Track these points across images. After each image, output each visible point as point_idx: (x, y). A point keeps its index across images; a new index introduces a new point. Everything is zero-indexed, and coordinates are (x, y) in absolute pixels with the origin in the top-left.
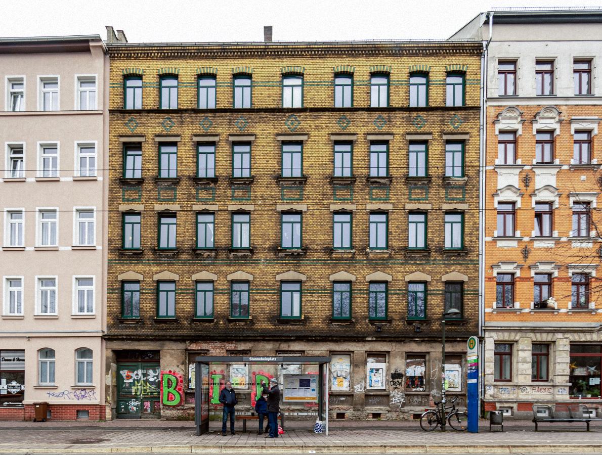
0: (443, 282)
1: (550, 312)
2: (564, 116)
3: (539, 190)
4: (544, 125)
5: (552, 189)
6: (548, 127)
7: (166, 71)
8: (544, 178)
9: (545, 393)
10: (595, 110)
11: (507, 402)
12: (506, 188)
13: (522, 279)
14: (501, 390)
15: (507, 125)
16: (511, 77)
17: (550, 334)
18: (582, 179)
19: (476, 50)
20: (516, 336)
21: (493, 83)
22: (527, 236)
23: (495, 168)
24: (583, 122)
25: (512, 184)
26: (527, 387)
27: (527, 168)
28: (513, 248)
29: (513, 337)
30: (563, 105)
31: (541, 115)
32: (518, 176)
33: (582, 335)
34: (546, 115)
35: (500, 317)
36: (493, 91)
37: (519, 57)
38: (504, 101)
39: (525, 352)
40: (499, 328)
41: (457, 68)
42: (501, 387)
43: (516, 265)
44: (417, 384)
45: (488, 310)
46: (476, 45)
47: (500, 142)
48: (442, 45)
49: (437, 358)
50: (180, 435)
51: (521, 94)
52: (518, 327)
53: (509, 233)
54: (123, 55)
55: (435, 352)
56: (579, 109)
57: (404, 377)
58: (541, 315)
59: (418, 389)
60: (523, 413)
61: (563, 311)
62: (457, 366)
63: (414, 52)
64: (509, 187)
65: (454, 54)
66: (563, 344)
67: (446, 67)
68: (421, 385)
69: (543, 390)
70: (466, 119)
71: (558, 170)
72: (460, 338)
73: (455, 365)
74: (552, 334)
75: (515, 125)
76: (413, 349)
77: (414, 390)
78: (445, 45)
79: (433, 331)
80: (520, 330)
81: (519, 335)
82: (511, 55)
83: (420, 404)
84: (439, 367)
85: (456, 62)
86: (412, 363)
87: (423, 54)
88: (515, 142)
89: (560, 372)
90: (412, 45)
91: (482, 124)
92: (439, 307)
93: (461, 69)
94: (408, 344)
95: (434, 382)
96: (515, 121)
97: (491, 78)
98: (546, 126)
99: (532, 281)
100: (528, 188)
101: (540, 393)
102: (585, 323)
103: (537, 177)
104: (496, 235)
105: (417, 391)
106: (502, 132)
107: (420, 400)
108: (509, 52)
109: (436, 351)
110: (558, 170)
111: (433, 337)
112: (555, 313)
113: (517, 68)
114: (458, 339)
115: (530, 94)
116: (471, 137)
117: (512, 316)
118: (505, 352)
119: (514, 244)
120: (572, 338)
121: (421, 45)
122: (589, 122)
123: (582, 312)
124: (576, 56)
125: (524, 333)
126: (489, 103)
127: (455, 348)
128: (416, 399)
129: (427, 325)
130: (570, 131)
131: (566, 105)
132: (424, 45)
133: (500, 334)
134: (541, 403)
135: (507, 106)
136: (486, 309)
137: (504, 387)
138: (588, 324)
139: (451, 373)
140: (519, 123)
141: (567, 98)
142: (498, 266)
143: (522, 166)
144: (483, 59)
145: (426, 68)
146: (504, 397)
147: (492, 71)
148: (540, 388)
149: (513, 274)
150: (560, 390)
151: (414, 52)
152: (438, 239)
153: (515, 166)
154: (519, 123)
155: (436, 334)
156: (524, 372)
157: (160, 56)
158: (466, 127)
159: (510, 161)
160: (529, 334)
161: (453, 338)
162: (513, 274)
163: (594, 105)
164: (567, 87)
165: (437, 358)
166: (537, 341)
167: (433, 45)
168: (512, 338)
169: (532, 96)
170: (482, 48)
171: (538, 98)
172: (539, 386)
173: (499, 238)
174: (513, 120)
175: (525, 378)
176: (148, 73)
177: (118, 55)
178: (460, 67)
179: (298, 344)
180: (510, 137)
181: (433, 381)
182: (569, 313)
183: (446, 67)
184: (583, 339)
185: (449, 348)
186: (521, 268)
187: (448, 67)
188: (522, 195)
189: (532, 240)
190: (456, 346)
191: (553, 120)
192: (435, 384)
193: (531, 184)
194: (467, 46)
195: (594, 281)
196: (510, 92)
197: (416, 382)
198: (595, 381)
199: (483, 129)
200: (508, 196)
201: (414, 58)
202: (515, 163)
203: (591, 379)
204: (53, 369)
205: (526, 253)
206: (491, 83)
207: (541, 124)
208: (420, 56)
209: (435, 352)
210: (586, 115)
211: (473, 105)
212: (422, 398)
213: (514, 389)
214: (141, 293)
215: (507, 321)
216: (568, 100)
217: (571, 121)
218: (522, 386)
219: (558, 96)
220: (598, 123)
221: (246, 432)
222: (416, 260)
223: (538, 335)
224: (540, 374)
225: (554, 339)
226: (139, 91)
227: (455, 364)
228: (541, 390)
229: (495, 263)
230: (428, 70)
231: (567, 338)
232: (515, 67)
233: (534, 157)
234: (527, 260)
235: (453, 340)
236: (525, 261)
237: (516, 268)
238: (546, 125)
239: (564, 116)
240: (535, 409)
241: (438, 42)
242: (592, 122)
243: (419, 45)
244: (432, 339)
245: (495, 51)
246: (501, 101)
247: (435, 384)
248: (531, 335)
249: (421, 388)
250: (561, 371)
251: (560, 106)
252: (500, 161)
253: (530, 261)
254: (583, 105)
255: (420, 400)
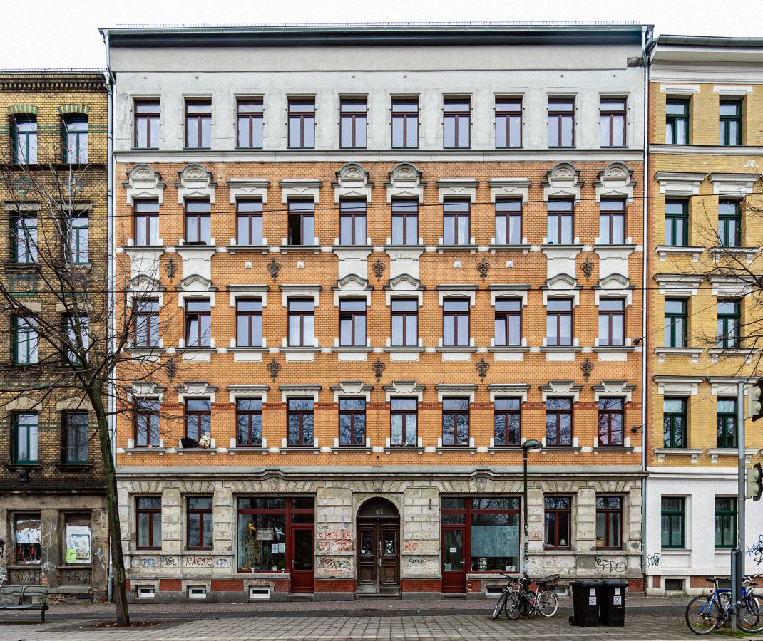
0: (58, 412)
1: (201, 453)
2: (221, 178)
3: (604, 281)
4: (611, 190)
5: (622, 279)
6: (617, 192)
7: (19, 109)
8: (196, 265)
9: (204, 565)
10: (261, 169)
11: (144, 579)
12: (558, 278)
13: (583, 406)
14: (143, 562)
15: (143, 191)
16: (618, 121)
17: (204, 483)
18: (455, 266)
19: (97, 83)
20: (304, 484)
21: (123, 131)
22: (484, 346)
23: (542, 250)
24: (454, 186)
25: (357, 274)
26: (174, 558)
27: (587, 249)
28: (255, 364)
29: (154, 487)
30: (218, 163)
31: (607, 174)
32: (365, 263)
33: (247, 484)
34: (613, 174)
35: (137, 460)
36: (124, 142)
37: (577, 93)
38: (139, 156)
39: (172, 508)
40: (129, 476)
41: (74, 109)
42: (143, 558)
43: (625, 385)
44: (33, 555)
45: (120, 450)
46: (93, 77)
47: (603, 213)
48: (45, 77)
49: (51, 518)
50: (332, 626)
51: (579, 146)
52: (155, 474)
53: (514, 342)
54: (85, 85)
55: (48, 509)
56: (448, 168)
57: (5, 545)
58: (192, 456)
59: (34, 562)
60: (167, 593)
61: (482, 449)
62: (86, 530)
63: (11, 86)
64: (403, 277)
65: (69, 90)
66: (223, 496)
67: (59, 108)
68: (38, 556)
69: (201, 561)
70: (88, 182)
71: (369, 253)
72: (76, 490)
73: (83, 527)
74: (207, 483)
75: (570, 188)
76: (17, 506)
77: (28, 562)
78: (50, 76)
79: (45, 479)
80: (158, 478)
81: (318, 484)
82: (149, 91)
83: (33, 582)
84: (53, 530)
85: (73, 101)
86: (25, 526)
87: (26, 89)
88: (623, 213)
89: (218, 536)
90: (5, 77)
91: (110, 188)
92: (53, 446)
93: (80, 111)
94: (9, 499)
95: (46, 551)
96: (623, 183)
97: (121, 124)
98: (614, 191)
99: (545, 408)
100: (173, 279)
101: (197, 565)
102: (253, 467)
103: (185, 264)
104: (597, 345)
105: (33, 564)
106: (605, 199)
107: (32, 576)
108: (147, 88)
109: (51, 507)
110: (369, 253)
111: (38, 489)
112: (419, 453)
113: (627, 109)
114: (73, 492)
115: (175, 146)
116: (95, 207)
117: (618, 457)
118: (148, 508)
119: (570, 356)
120: (234, 489)
121: (16, 77)
122: (254, 186)
123: (248, 453)
124: (238, 93)
125: (169, 482)
126: (120, 160)
127: (74, 504)
128: (27, 576)
129: (36, 471)
130: (228, 200)
131: (223, 162)
132: (21, 77)
133: (136, 483)
134: (191, 579)
135: (556, 162)
136: (118, 449)
137: (147, 558)
138: (255, 469)
139: (79, 539)
140: (628, 185)
141: (223, 153)
142: (339, 389)
143: (581, 246)
144: (109, 97)
145: (32, 109)
146: (147, 571)
147: (122, 115)
148: (197, 558)
149: (623, 398)
150: (219, 562)
151: (11, 86)
152: (51, 351)
153: (571, 247)
154: (628, 185)
155: (49, 484)
156: (169, 537)
157: (31, 88)
158: (88, 192)
159: (617, 239)
160: (176, 483)
161: (65, 489)
162: (623, 398)
163: (262, 163)
164: (224, 136)
165: (51, 518)
166: (194, 493)
167: (33, 76)
168: (568, 489)
169: (176, 149)
170: (103, 81)
171: (552, 150)
172: (195, 556)
173: (498, 349)
174: (150, 183)
175: (172, 545)
176: (44, 111)
177: (78, 85)
178: (78, 109)
179: (52, 500)
180: (618, 206)
181: (45, 549)
182: (491, 453)
183: (59, 108)
184: (457, 489)
185: (19, 504)
186: (580, 390)
187: (62, 108)
188: (581, 289)
189: (492, 351)
190: (76, 501)
191: (571, 182)
192: (47, 554)
193: (177, 274)
194: (83, 79)
195: (630, 409)
196: (618, 142)
197: (31, 552)
198: (279, 548)
199: (112, 197)
200: (560, 288)
201: (14, 95)
202: (573, 243)
203: (273, 545)
204: (193, 532)
205: (587, 368)
206: (121, 131)
207: (606, 188)
208: (23, 93)
209: (48, 509)
210: (251, 176)
211: (97, 162)
212: (35, 574)
213: (162, 561)
214: (40, 429)
215: (146, 464)
216: (538, 155)
217: (229, 185)
218: (168, 555)
219: (212, 150)
220: (529, 188)
221: (129, 624)
222: (21, 381)
223: (188, 485)
224: (198, 537)
225: (210, 490)
226: (33, 138)
227: (84, 525)
228: (198, 561)
229: (545, 384)
230: (34, 112)
231: (228, 488)
232: (625, 107)
233: (546, 235)
234: (381, 379)
235: (66, 492)
236: (274, 381)
237: (156, 390)
238: (353, 190)
239: (221, 178)
240: (184, 589)
241: (82, 72)
242: (258, 187)
243: (14, 77)
244: (39, 493)
245: (128, 86)
246: (135, 156)
247: (47, 554)
248: (179, 484)
249: (38, 559)
250: (219, 534)
251: (215, 163)
252: (602, 239)
253: (385, 380)
254: (247, 163)
255: (32, 576)
